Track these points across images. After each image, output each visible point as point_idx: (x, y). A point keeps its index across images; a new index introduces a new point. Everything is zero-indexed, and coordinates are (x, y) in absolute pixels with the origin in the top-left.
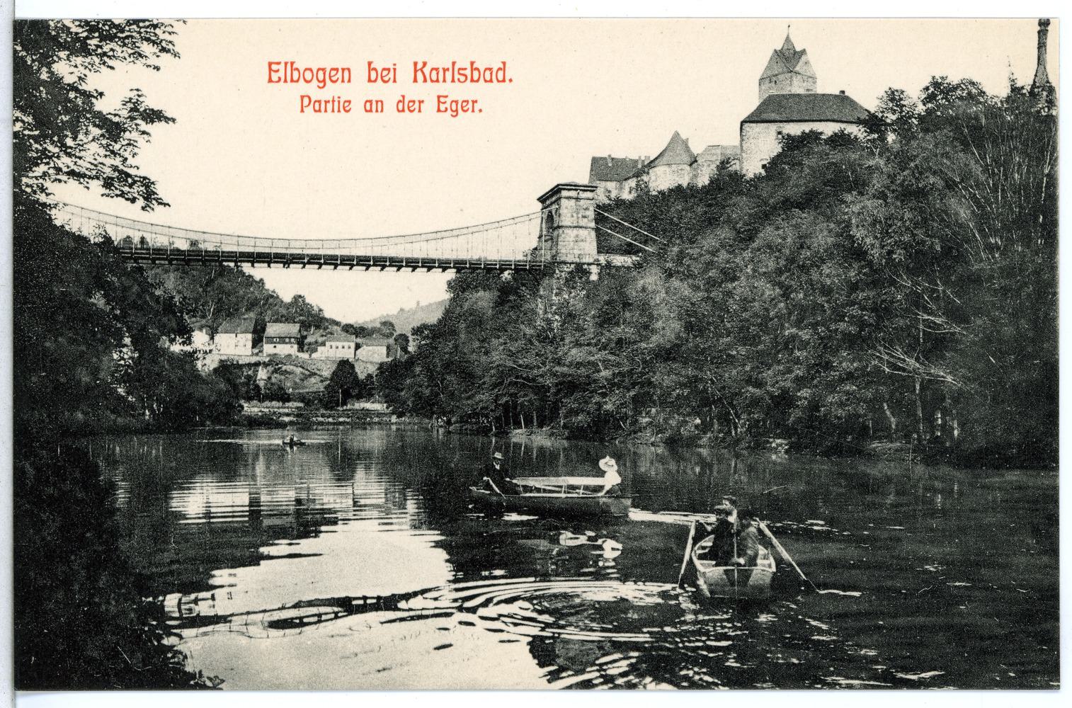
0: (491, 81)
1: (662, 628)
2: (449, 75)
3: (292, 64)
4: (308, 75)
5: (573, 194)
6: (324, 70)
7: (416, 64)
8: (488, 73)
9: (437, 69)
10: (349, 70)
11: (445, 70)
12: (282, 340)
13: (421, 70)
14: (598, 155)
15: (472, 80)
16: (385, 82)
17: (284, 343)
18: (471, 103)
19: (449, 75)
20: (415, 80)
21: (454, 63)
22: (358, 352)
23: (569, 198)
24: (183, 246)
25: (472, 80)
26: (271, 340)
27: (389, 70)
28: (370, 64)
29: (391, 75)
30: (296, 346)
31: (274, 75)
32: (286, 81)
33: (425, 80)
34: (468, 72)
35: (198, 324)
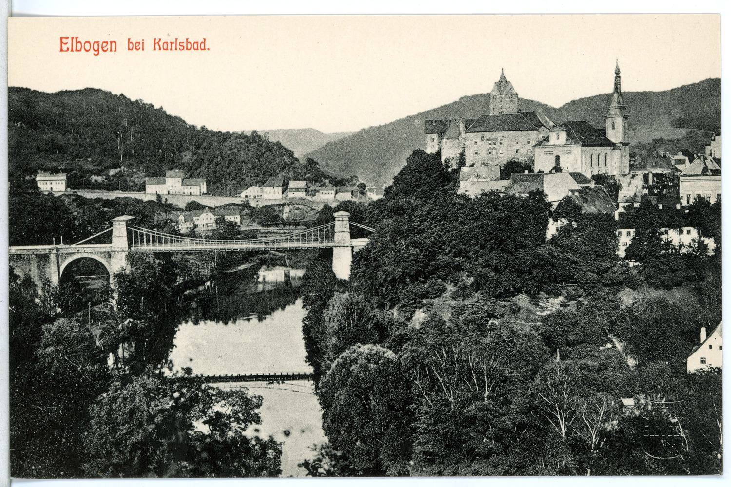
0: (197, 49)
1: (197, 288)
2: (174, 46)
3: (77, 38)
4: (87, 46)
5: (341, 219)
6: (197, 43)
7: (155, 40)
8: (196, 45)
9: (167, 43)
10: (115, 42)
11: (172, 43)
12: (297, 190)
13: (158, 43)
14: (124, 94)
15: (187, 49)
16: (137, 49)
17: (298, 191)
18: (109, 44)
19: (174, 46)
20: (155, 49)
21: (176, 40)
22: (337, 196)
23: (339, 220)
24: (249, 134)
25: (187, 49)
26: (292, 190)
27: (139, 43)
28: (129, 40)
29: (141, 46)
30: (304, 193)
31: (65, 47)
32: (72, 50)
33: (160, 49)
34: (185, 45)
35: (254, 181)
